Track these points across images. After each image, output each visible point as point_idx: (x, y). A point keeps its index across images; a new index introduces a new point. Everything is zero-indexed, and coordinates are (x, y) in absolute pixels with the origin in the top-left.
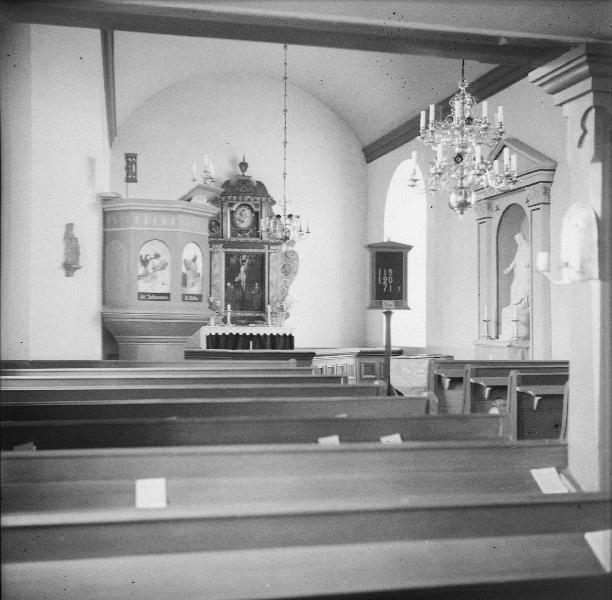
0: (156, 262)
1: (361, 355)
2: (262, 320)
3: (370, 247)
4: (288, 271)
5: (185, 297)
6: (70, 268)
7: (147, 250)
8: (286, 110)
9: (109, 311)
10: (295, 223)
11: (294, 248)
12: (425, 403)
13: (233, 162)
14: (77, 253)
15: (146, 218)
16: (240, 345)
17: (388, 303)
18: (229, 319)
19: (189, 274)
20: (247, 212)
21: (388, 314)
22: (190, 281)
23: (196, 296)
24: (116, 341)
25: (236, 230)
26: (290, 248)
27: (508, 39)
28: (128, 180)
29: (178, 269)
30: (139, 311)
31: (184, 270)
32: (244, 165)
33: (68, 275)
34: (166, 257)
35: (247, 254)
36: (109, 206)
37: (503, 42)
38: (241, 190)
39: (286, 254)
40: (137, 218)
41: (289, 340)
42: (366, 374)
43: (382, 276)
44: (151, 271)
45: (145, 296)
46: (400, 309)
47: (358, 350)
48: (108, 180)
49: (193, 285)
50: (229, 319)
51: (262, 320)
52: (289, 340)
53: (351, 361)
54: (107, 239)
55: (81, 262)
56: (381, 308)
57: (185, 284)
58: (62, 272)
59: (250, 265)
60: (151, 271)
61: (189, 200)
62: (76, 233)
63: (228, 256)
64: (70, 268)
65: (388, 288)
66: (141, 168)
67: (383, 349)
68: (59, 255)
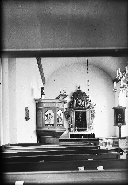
0: (50, 116)
1: (113, 139)
2: (86, 130)
3: (114, 108)
4: (92, 116)
5: (58, 125)
6: (27, 119)
7: (48, 113)
8: (88, 73)
9: (38, 130)
10: (92, 103)
11: (94, 110)
12: (116, 155)
13: (76, 87)
14: (29, 115)
15: (47, 104)
16: (80, 137)
17: (119, 124)
18: (76, 130)
19: (59, 119)
20: (81, 100)
21: (120, 127)
22: (60, 120)
23: (62, 125)
24: (41, 137)
25: (78, 105)
26: (93, 109)
27: (118, 49)
28: (42, 94)
29: (56, 118)
30: (46, 129)
31: (58, 118)
32: (79, 88)
33: (26, 121)
34: (53, 114)
35: (81, 112)
36: (37, 102)
37: (116, 51)
38: (78, 95)
39: (92, 111)
40: (44, 104)
41: (93, 135)
42: (115, 144)
43: (118, 116)
44: (49, 118)
45: (47, 125)
46: (124, 125)
47: (113, 137)
48: (38, 95)
49: (60, 122)
50: (76, 130)
51: (86, 130)
52: (93, 135)
53: (111, 141)
54: (37, 110)
55: (30, 117)
56: (117, 125)
57: (58, 121)
58: (25, 120)
59: (82, 115)
60: (49, 118)
61: (59, 99)
62: (28, 109)
63: (76, 112)
64: (27, 119)
65: (120, 119)
66: (46, 91)
67: (119, 137)
68: (24, 116)
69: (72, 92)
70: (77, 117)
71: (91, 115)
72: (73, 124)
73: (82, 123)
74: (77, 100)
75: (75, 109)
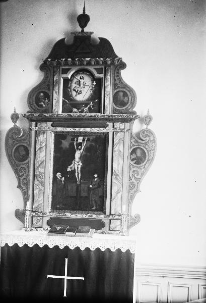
4: (140, 156)
11: (150, 127)
20: (87, 80)
25: (70, 103)
26: (144, 127)
32: (83, 19)
35: (84, 134)
59: (87, 150)
63: (59, 137)
69: (50, 43)
70: (62, 158)
71: (134, 151)
72: (45, 196)
73: (83, 191)
74: (71, 80)
75: (57, 121)
